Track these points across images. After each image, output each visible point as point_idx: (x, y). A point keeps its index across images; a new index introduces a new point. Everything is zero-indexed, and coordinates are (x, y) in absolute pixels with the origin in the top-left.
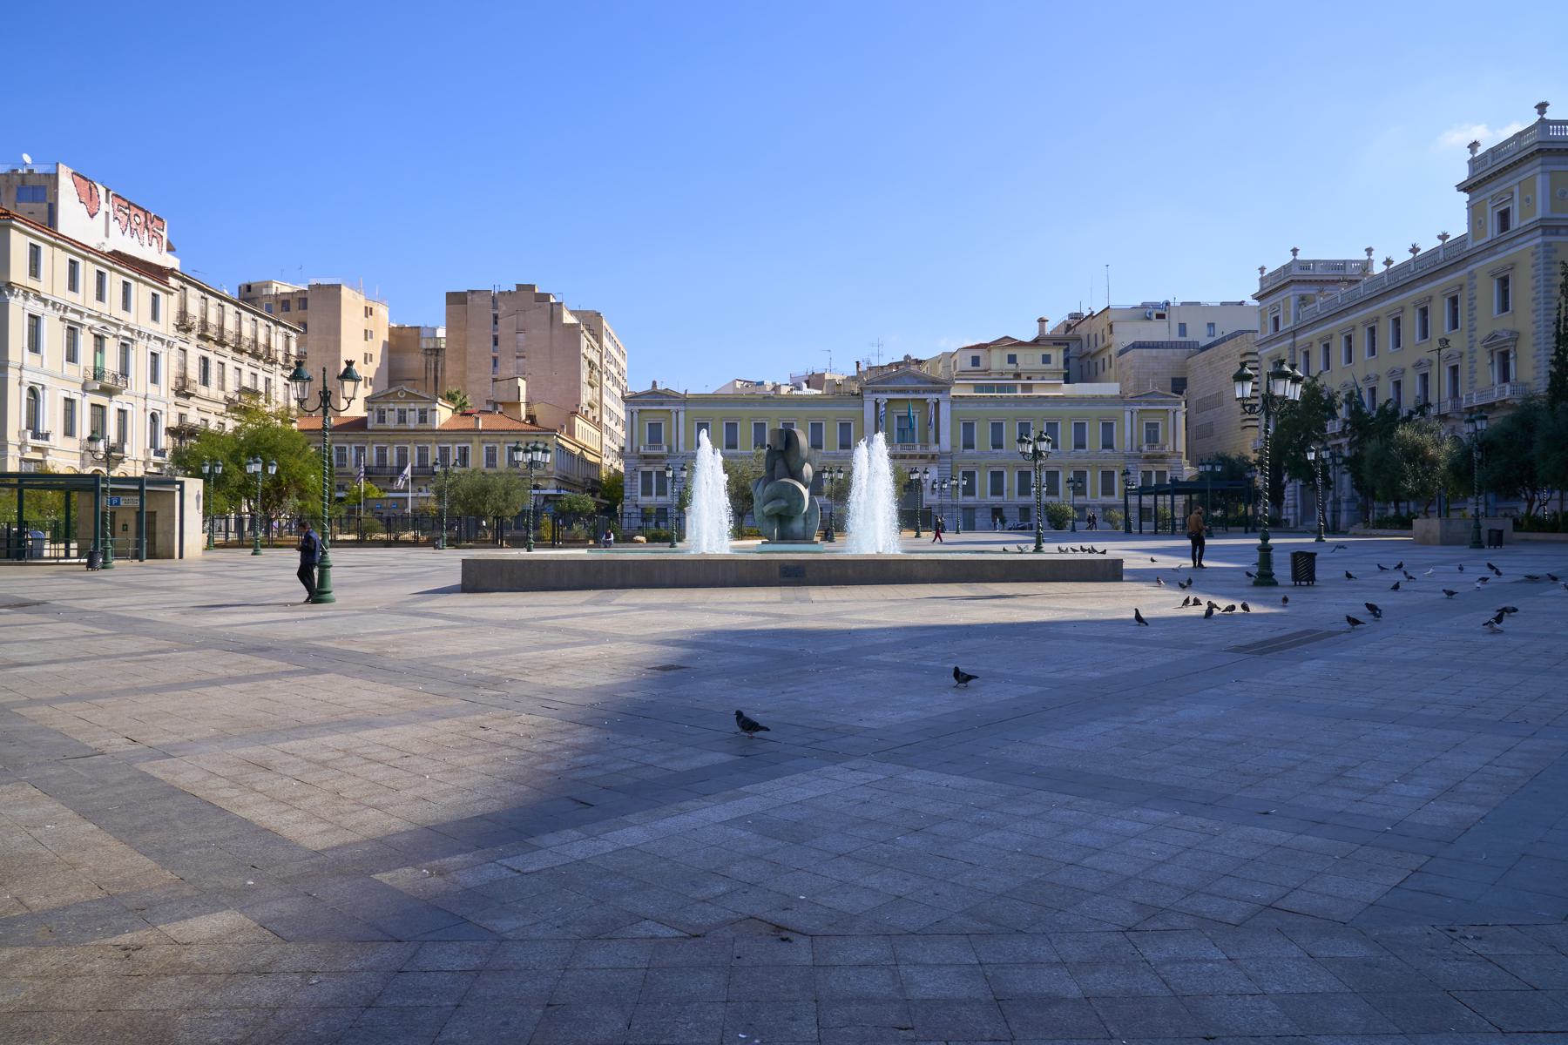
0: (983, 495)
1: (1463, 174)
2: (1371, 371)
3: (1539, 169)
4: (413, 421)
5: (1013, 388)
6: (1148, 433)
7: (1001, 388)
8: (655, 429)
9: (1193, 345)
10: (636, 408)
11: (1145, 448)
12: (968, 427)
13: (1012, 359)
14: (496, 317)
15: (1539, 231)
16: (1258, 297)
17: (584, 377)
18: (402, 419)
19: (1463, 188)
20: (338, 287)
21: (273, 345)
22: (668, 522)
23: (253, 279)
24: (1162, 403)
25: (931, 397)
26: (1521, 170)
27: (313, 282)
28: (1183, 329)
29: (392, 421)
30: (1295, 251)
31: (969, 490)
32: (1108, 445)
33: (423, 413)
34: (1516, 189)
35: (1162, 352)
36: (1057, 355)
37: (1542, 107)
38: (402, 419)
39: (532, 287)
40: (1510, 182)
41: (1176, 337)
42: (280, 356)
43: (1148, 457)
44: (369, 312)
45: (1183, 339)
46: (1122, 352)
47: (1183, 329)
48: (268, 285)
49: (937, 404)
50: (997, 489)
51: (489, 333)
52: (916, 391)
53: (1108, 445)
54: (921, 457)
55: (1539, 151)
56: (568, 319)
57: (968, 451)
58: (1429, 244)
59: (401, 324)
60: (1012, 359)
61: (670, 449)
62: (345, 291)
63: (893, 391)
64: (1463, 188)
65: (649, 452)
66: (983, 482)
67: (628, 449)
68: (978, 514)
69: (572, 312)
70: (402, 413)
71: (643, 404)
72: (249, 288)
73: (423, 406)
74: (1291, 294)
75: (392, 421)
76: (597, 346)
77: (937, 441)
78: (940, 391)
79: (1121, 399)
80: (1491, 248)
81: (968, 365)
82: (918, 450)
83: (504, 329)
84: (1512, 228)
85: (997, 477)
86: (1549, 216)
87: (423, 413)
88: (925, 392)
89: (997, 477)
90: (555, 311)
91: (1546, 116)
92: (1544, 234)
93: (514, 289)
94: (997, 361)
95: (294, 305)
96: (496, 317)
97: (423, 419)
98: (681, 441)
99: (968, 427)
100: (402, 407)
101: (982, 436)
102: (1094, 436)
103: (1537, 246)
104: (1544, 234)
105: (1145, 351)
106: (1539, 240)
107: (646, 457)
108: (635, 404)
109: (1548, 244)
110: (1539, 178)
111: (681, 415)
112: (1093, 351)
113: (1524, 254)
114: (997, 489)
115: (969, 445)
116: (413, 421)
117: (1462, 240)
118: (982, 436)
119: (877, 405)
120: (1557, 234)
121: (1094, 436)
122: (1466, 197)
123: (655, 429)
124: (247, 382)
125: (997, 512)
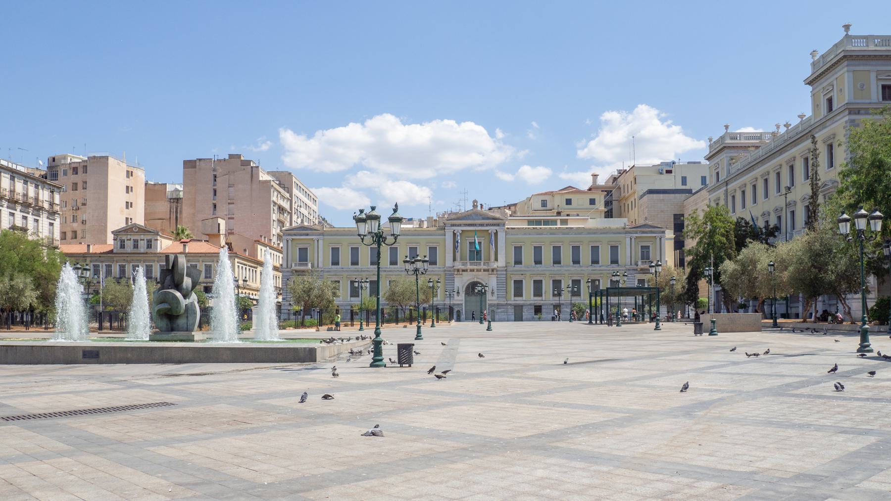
0: (528, 296)
1: (808, 72)
2: (766, 209)
3: (846, 69)
4: (142, 245)
5: (554, 222)
6: (642, 253)
7: (546, 222)
8: (303, 255)
9: (689, 191)
10: (290, 238)
11: (640, 263)
12: (518, 250)
13: (569, 202)
14: (215, 176)
15: (847, 112)
16: (709, 158)
17: (274, 217)
18: (136, 246)
19: (811, 82)
20: (107, 158)
21: (41, 198)
22: (41, 315)
23: (56, 153)
24: (652, 232)
25: (492, 229)
26: (837, 69)
27: (92, 155)
28: (684, 180)
29: (129, 245)
30: (727, 127)
31: (518, 292)
32: (615, 261)
33: (149, 241)
34: (835, 83)
35: (661, 196)
36: (600, 199)
37: (847, 27)
38: (136, 246)
39: (239, 156)
40: (831, 78)
41: (680, 186)
42: (46, 206)
43: (642, 269)
44: (129, 174)
45: (684, 187)
46: (642, 197)
47: (684, 180)
48: (65, 158)
49: (496, 234)
50: (538, 292)
51: (210, 187)
52: (482, 225)
53: (615, 261)
54: (484, 270)
55: (845, 57)
56: (263, 177)
57: (518, 267)
58: (795, 122)
59: (156, 182)
60: (569, 202)
61: (313, 266)
62: (111, 161)
63: (466, 225)
64: (811, 82)
65: (298, 268)
66: (528, 288)
67: (285, 266)
68: (525, 310)
69: (268, 173)
70: (136, 242)
71: (295, 235)
72: (54, 159)
73: (149, 237)
74: (724, 157)
75: (129, 245)
76: (287, 195)
77: (496, 259)
78: (498, 225)
79: (624, 231)
80: (822, 125)
81: (538, 205)
82: (483, 267)
83: (221, 185)
84: (834, 109)
85: (538, 284)
86: (853, 101)
87: (149, 241)
88: (487, 225)
89: (538, 284)
90: (253, 173)
91: (850, 33)
92: (850, 113)
93: (227, 158)
94: (559, 201)
95: (80, 170)
96: (215, 176)
97: (149, 246)
98: (321, 259)
99: (518, 250)
100: (136, 237)
101: (528, 256)
102: (605, 256)
103: (846, 122)
104: (850, 113)
105: (655, 196)
106: (847, 118)
107: (296, 271)
108: (290, 235)
109: (852, 121)
110: (846, 75)
111: (321, 242)
112: (627, 195)
113: (839, 127)
114: (538, 292)
115: (518, 262)
116: (142, 245)
117: (810, 119)
118: (528, 256)
119: (454, 234)
120: (859, 113)
121: (605, 256)
122: (810, 88)
123: (303, 255)
124: (19, 223)
125: (538, 310)
